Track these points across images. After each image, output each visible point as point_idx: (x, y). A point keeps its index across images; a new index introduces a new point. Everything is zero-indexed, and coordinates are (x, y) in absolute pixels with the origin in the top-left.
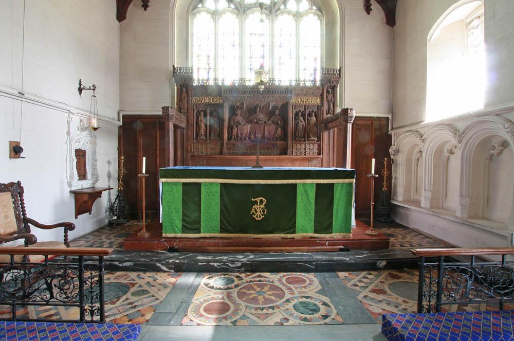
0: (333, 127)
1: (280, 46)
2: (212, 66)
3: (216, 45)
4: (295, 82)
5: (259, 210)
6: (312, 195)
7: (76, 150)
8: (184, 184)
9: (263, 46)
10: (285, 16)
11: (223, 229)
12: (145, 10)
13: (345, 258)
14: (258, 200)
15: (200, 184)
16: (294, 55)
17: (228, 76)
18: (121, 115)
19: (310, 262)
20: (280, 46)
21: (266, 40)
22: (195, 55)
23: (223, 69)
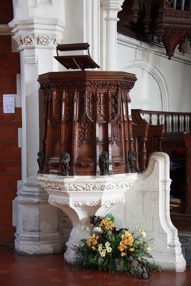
7: (131, 110)
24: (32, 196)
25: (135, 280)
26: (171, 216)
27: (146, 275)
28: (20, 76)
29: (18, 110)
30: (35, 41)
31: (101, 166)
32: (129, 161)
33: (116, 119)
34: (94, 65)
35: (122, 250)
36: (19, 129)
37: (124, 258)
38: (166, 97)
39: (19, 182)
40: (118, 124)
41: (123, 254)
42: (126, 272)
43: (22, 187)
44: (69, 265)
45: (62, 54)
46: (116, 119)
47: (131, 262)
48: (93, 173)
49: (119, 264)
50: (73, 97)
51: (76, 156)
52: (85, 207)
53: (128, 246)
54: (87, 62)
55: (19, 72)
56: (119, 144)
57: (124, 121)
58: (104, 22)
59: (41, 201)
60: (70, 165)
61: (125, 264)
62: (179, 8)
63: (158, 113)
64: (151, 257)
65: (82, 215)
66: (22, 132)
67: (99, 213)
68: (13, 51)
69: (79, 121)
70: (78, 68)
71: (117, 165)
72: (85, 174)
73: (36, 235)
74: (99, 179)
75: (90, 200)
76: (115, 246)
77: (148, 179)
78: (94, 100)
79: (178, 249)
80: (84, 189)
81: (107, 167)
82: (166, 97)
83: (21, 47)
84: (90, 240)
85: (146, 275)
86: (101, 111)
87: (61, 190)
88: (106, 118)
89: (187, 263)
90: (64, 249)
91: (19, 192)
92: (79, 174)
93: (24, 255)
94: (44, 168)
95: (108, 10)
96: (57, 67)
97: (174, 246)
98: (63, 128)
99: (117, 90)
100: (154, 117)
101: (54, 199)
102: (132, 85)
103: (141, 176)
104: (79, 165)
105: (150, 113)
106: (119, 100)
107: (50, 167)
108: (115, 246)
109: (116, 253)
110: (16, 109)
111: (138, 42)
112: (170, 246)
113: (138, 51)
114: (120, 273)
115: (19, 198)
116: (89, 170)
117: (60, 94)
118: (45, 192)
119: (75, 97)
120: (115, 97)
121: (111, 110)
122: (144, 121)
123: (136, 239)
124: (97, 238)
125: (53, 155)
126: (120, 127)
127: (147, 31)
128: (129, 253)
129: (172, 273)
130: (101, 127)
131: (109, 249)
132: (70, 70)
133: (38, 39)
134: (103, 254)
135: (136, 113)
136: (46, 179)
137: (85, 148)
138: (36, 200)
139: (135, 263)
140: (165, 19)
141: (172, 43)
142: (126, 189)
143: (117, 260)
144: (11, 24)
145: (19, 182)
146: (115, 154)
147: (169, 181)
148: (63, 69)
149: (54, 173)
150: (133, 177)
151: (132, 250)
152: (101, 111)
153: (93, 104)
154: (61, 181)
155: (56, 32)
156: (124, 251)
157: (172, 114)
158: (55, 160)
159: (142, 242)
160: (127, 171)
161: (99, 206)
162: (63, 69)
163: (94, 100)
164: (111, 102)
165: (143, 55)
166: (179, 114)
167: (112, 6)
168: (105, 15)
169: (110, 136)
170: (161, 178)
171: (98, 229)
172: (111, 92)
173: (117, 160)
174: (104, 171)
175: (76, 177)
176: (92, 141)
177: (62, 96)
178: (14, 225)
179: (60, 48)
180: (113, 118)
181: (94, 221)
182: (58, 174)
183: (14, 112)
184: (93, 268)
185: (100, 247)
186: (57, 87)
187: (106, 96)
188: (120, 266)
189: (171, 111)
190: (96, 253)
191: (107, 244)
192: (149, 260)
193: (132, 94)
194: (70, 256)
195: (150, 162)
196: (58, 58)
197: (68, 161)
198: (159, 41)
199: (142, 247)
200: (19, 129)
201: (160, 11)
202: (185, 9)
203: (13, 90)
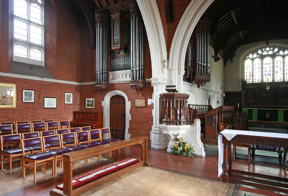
0: (199, 112)
1: (277, 67)
2: (251, 75)
3: (253, 69)
4: (218, 194)
5: (268, 116)
6: (283, 113)
7: (151, 98)
8: (248, 109)
9: (270, 67)
10: (279, 57)
11: (258, 120)
12: (232, 63)
13: (220, 28)
14: (267, 113)
15: (252, 109)
16: (282, 69)
17: (257, 79)
18: (225, 92)
19: (281, 127)
20: (277, 67)
21: (271, 65)
22: (245, 72)
23: (255, 76)
24: (157, 131)
25: (190, 158)
26: (201, 139)
27: (193, 157)
28: (153, 94)
29: (152, 104)
30: (158, 84)
31: (179, 122)
32: (187, 121)
33: (183, 108)
34: (177, 92)
35: (185, 149)
36: (153, 110)
37: (186, 151)
38: (197, 100)
39: (152, 126)
40: (184, 110)
41: (186, 150)
42: (187, 156)
43: (153, 128)
44: (169, 153)
45: (167, 88)
46: (183, 108)
47: (188, 153)
48: (177, 124)
49: (185, 153)
50: (170, 101)
51: (171, 119)
52: (174, 135)
53: (187, 148)
54: (175, 91)
55: (153, 92)
56: (184, 115)
57: (186, 109)
58: (179, 78)
59: (159, 132)
60: (169, 122)
61: (186, 154)
62: (201, 74)
63: (195, 105)
64: (195, 152)
65: (173, 138)
66: (154, 111)
67: (178, 137)
68: (151, 86)
69: (172, 108)
70: (172, 92)
71: (184, 122)
72: (174, 125)
73: (158, 143)
74: (178, 126)
75: (176, 133)
76: (183, 148)
77: (194, 127)
78: (177, 102)
79: (203, 150)
80: (174, 129)
81: (181, 123)
82: (197, 100)
83: (154, 86)
84: (175, 145)
85: (193, 157)
86: (179, 105)
87: (166, 129)
88: (181, 107)
89: (206, 154)
90: (166, 148)
91: (152, 129)
92: (172, 124)
93: (154, 149)
94: (161, 122)
95: (180, 75)
96: (165, 92)
97: (202, 149)
98: (167, 110)
99: (184, 99)
100: (194, 107)
101: (165, 132)
102: (188, 97)
103: (192, 126)
104: (172, 122)
105: (193, 105)
106: (184, 102)
107: (163, 122)
108: (183, 148)
109: (184, 150)
110: (152, 103)
111: (189, 83)
112: (200, 148)
113: (189, 86)
114: (185, 156)
115: (152, 131)
116: (175, 123)
117: (166, 100)
118: (161, 130)
119: (171, 101)
120: (183, 101)
121: (182, 105)
122: (191, 108)
123: (190, 146)
124: (178, 145)
125: (164, 118)
126: (185, 110)
127: (191, 80)
128: (188, 150)
129: (201, 157)
130: (179, 110)
131: (182, 149)
132: (170, 93)
133: (159, 83)
134: (180, 150)
135: (189, 105)
136: (162, 126)
137: (174, 116)
138: (158, 132)
139: (190, 153)
140: (197, 77)
141: (199, 84)
142: (186, 130)
143: (184, 152)
144: (151, 79)
145: (152, 126)
146: (281, 70)
147: (200, 128)
148: (167, 92)
149: (164, 124)
150: (189, 126)
151: (189, 149)
152: (179, 105)
153: (176, 103)
154: (167, 126)
155: (165, 81)
156: (273, 50)
157: (200, 106)
158: (164, 120)
159: (192, 147)
160: (187, 124)
161: (178, 135)
162: (167, 92)
163: (177, 102)
164: (182, 102)
165: (190, 87)
166: (202, 106)
167: (181, 74)
168: (179, 76)
169: (182, 113)
170: (198, 127)
171: (178, 142)
172: (182, 99)
173: (184, 121)
174: (180, 124)
175: (171, 125)
176: (176, 115)
177: (167, 101)
178: (150, 139)
179: (167, 87)
180: (183, 108)
181: (177, 140)
182: (166, 124)
183: (45, 98)
184: (176, 154)
185: (179, 148)
186: (165, 98)
187: (180, 101)
188: (185, 154)
189: (199, 104)
190: (177, 150)
191: (181, 147)
192: (194, 153)
193: (188, 100)
194: (169, 150)
195: (194, 122)
196: (166, 90)
197: (169, 120)
198: (195, 83)
199: (192, 149)
200: (153, 110)
201: (195, 74)
202: (203, 74)
203: (151, 98)
